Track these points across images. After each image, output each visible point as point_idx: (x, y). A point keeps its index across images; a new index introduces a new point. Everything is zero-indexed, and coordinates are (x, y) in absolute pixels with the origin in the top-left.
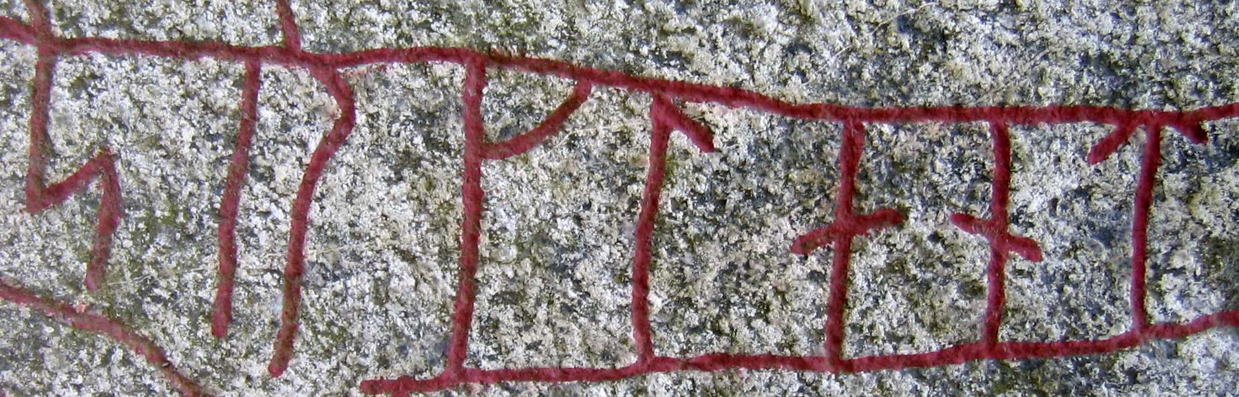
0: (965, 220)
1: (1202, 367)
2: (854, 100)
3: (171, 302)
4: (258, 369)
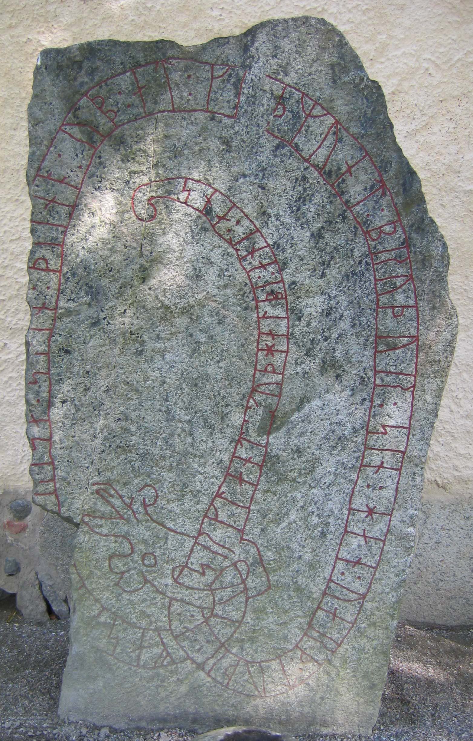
0: (244, 465)
1: (273, 441)
2: (225, 473)
3: (222, 563)
4: (233, 555)
